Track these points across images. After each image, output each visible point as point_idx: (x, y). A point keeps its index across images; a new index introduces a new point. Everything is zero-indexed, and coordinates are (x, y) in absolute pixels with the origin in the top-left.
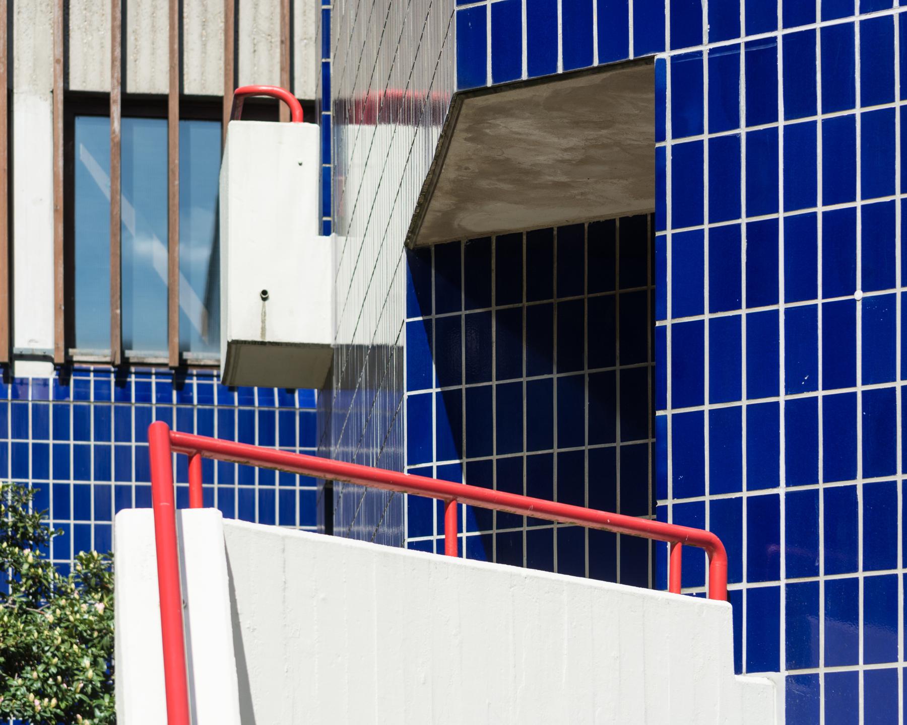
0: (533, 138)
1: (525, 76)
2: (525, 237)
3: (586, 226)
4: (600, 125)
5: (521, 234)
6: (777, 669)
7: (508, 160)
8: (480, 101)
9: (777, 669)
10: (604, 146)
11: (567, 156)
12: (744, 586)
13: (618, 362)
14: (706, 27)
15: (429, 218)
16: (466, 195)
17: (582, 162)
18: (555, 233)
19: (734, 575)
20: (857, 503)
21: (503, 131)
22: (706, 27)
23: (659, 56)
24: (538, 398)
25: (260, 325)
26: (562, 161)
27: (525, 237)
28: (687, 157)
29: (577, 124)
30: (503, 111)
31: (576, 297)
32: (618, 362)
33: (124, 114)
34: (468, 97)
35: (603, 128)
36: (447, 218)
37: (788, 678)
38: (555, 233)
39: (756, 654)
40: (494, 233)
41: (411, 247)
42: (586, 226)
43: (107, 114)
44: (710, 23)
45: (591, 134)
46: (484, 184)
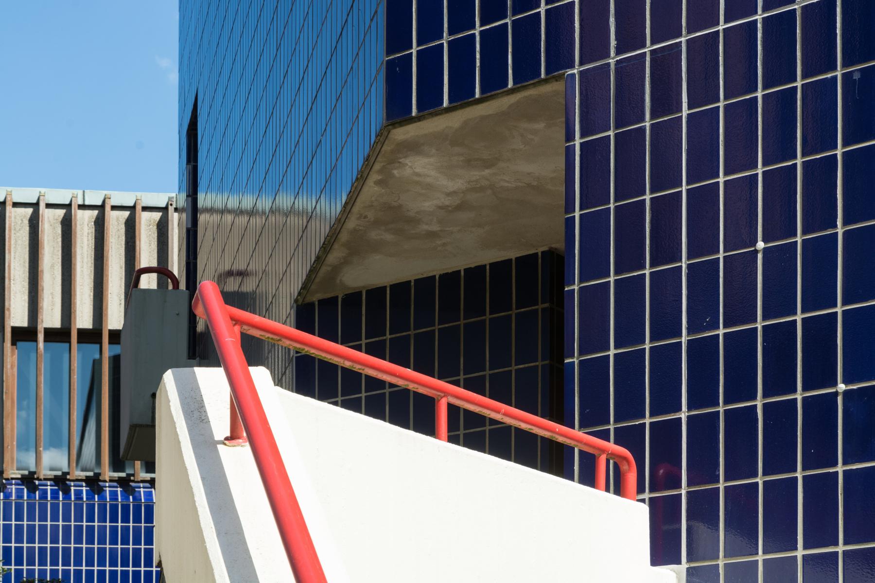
0: (428, 180)
1: (446, 103)
2: (388, 289)
3: (437, 277)
4: (487, 164)
5: (386, 287)
6: (679, 563)
7: (400, 206)
8: (401, 134)
9: (679, 563)
10: (482, 189)
11: (447, 201)
12: (646, 495)
13: (462, 373)
14: (613, 43)
15: (324, 270)
16: (359, 247)
17: (460, 207)
18: (412, 284)
19: (641, 489)
20: (757, 420)
21: (408, 172)
22: (613, 43)
23: (570, 72)
24: (468, 344)
25: (151, 415)
26: (441, 208)
27: (388, 289)
28: (593, 153)
29: (469, 163)
30: (413, 147)
31: (429, 329)
32: (462, 373)
33: (46, 340)
34: (395, 128)
35: (487, 167)
36: (336, 269)
37: (688, 570)
38: (412, 284)
39: (663, 551)
40: (364, 287)
41: (300, 303)
42: (437, 277)
43: (35, 340)
44: (616, 39)
45: (476, 174)
46: (374, 235)
